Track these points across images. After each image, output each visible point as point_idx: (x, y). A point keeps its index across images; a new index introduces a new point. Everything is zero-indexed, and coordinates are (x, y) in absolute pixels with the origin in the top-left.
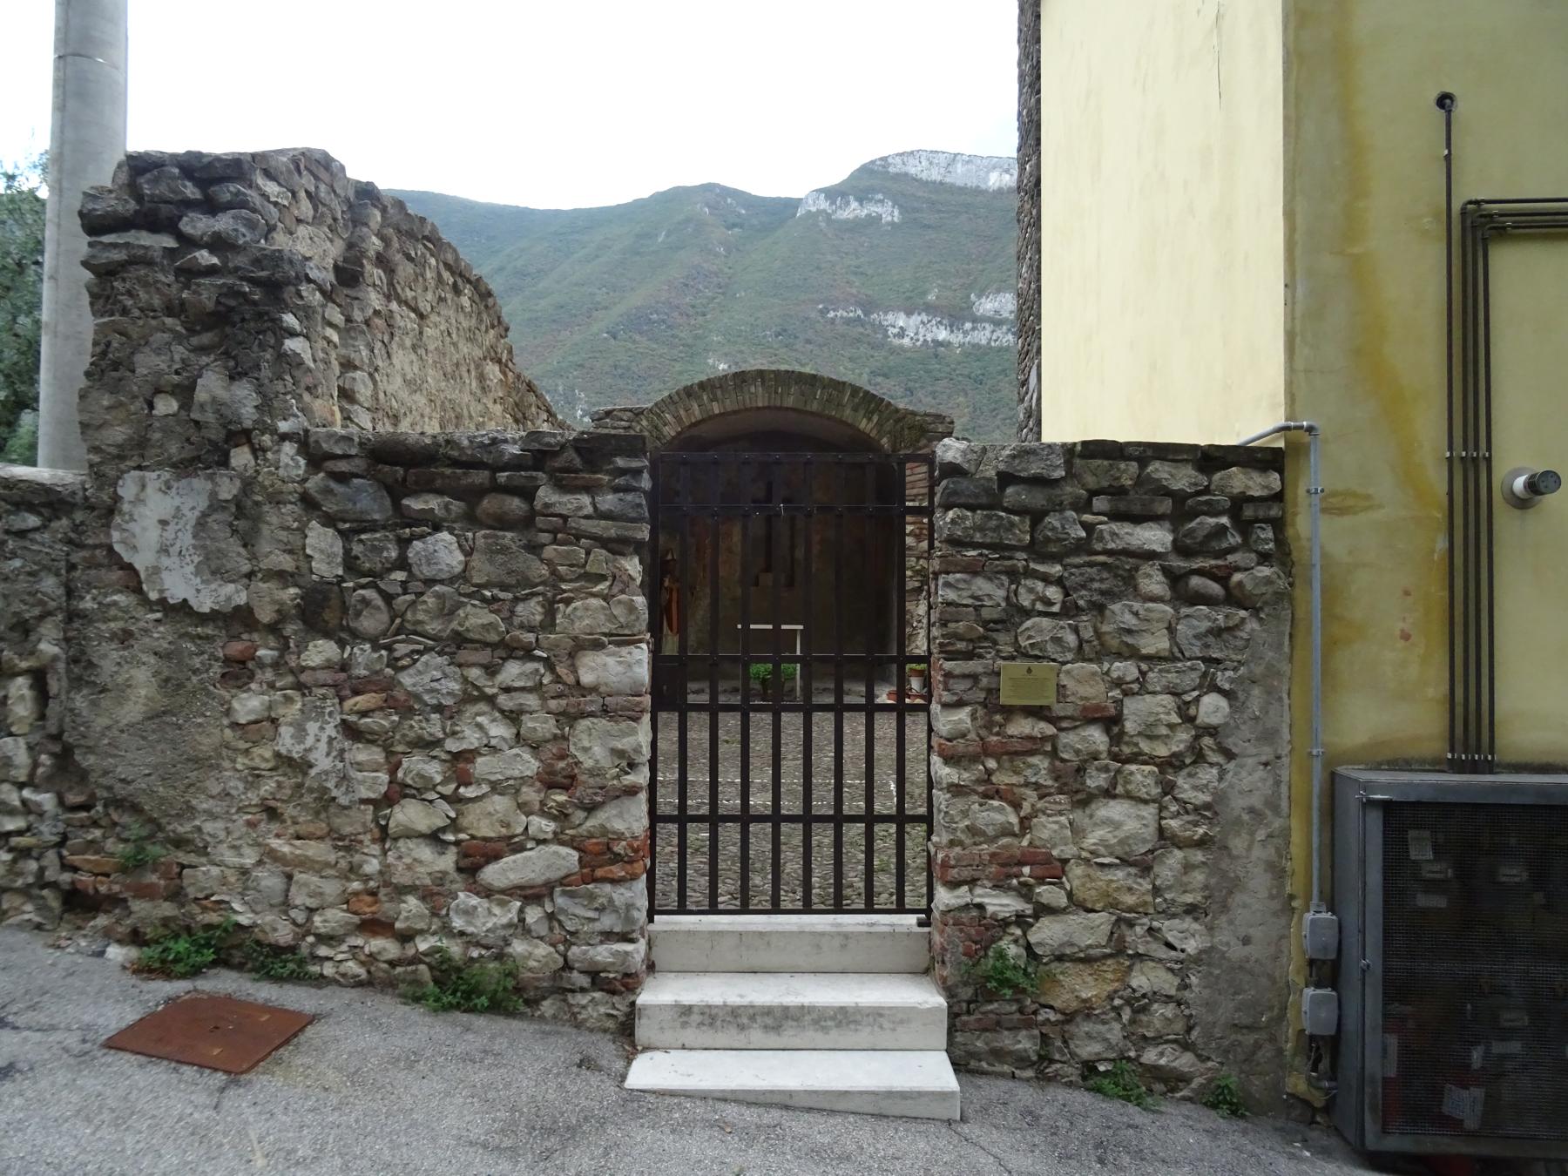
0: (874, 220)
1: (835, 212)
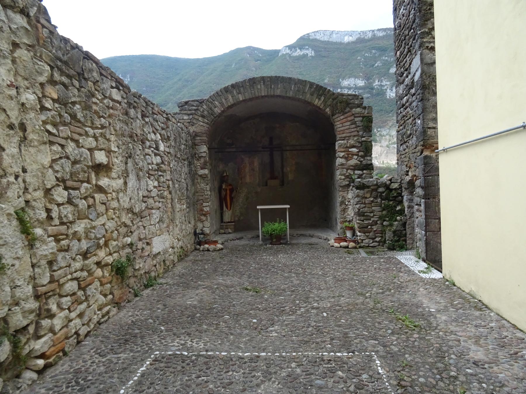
0: (305, 56)
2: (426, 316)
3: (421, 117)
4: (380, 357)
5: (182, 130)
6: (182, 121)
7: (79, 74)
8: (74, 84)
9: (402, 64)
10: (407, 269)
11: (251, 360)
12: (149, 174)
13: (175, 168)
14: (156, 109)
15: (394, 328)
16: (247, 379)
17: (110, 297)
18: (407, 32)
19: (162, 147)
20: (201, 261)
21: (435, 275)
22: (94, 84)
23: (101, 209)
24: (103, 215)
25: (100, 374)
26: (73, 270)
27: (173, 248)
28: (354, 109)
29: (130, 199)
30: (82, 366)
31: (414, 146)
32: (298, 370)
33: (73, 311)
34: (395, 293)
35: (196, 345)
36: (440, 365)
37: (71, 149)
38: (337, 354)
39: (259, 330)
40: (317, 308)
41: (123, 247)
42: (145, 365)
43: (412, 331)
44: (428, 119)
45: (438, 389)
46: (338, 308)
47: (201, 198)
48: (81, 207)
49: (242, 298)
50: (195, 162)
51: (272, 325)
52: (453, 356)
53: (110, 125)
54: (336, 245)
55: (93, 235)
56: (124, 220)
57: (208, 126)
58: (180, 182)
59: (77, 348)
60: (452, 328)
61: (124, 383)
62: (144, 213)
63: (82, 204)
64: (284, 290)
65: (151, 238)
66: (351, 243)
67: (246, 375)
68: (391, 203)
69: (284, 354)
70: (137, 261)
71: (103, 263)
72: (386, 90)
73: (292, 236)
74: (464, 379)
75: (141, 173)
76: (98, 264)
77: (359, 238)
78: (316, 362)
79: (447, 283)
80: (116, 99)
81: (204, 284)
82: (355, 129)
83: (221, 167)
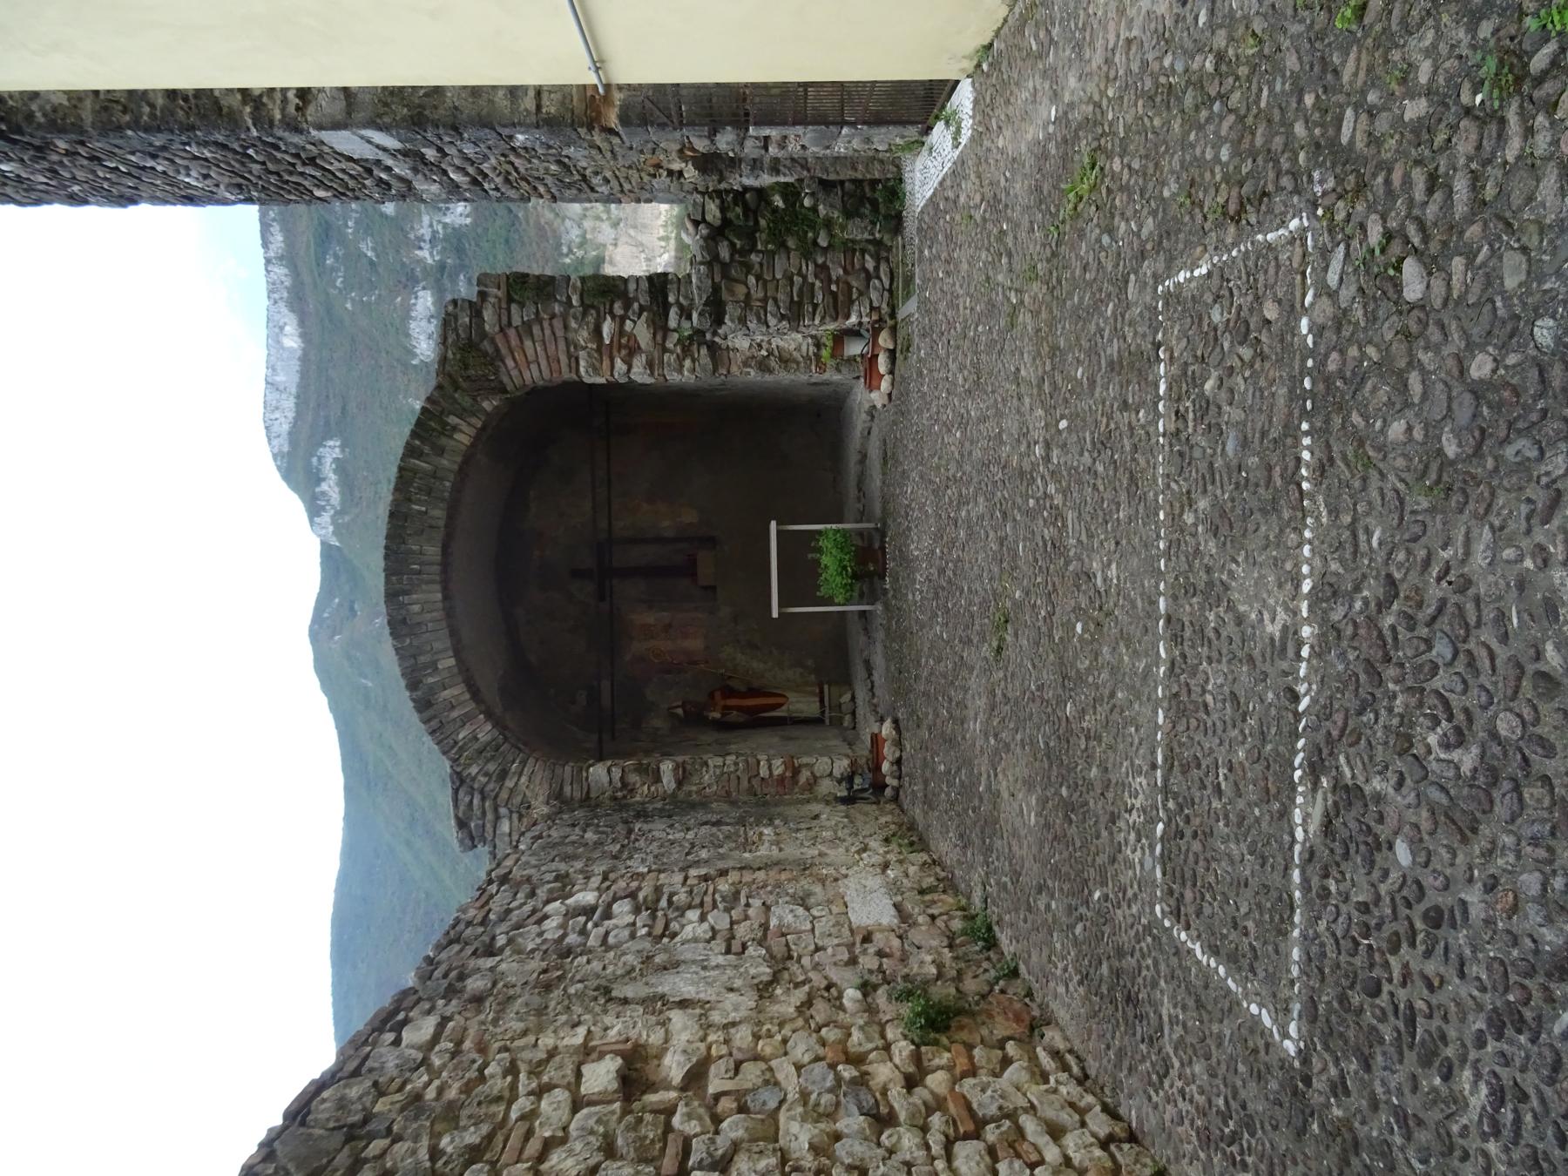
0: (341, 467)
1: (333, 507)
2: (1068, 133)
3: (506, 132)
4: (1170, 271)
5: (540, 837)
6: (515, 837)
7: (350, 1138)
8: (377, 1152)
9: (351, 183)
10: (948, 183)
11: (1176, 639)
12: (663, 935)
13: (650, 858)
14: (472, 913)
15: (1098, 225)
16: (1224, 651)
17: (1011, 1048)
18: (256, 168)
19: (587, 897)
20: (926, 783)
21: (964, 98)
22: (382, 1094)
23: (752, 1074)
24: (771, 1069)
25: (1213, 1075)
26: (923, 1153)
27: (885, 866)
28: (487, 327)
29: (731, 990)
30: (1192, 1125)
31: (594, 152)
32: (1203, 504)
33: (1040, 1153)
34: (1009, 220)
35: (1141, 796)
36: (1189, 100)
37: (570, 1162)
38: (1161, 392)
39: (1102, 615)
40: (1048, 446)
41: (871, 1010)
42: (1189, 944)
43: (1104, 176)
44: (512, 112)
45: (1248, 109)
46: (1047, 387)
47: (745, 784)
48: (740, 1133)
49: (1021, 665)
50: (638, 798)
51: (1089, 576)
52: (1167, 62)
53: (506, 1049)
54: (885, 385)
55: (827, 1099)
56: (792, 1009)
57: (531, 761)
58: (693, 845)
59: (1147, 1142)
60: (1098, 59)
61: (1233, 1008)
62: (775, 949)
63: (733, 1127)
64: (1001, 541)
65: (852, 931)
66: (881, 341)
67: (1215, 655)
68: (763, 223)
69: (1162, 546)
70: (915, 970)
71: (911, 1069)
72: (445, 226)
73: (862, 513)
74: (1222, 33)
75: (657, 960)
76: (911, 1083)
77: (865, 320)
78: (1181, 454)
79: (985, 67)
80: (431, 1030)
81: (985, 776)
82: (546, 324)
83: (658, 723)
